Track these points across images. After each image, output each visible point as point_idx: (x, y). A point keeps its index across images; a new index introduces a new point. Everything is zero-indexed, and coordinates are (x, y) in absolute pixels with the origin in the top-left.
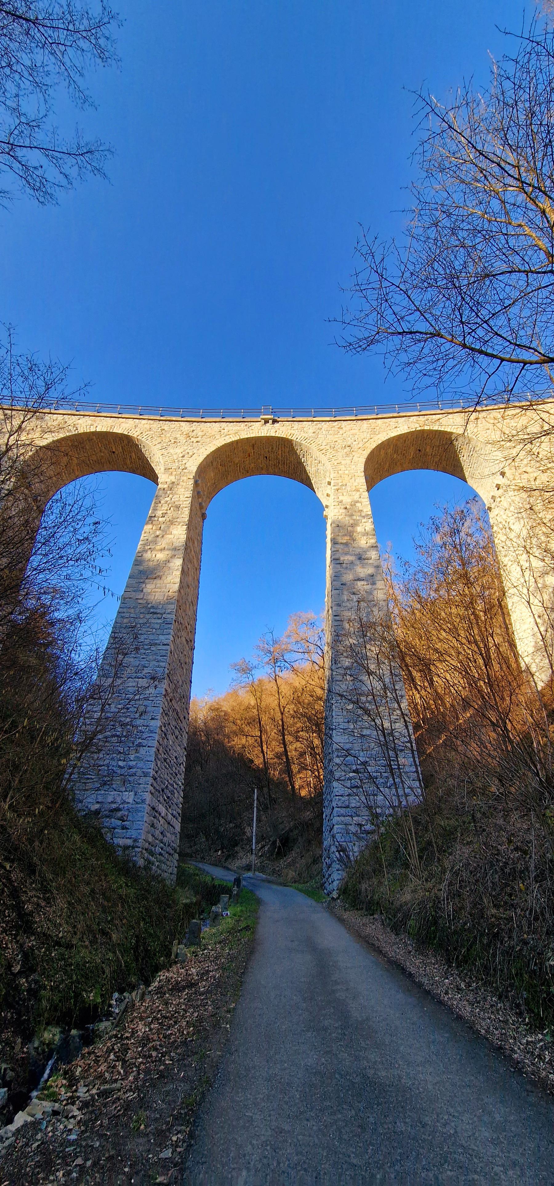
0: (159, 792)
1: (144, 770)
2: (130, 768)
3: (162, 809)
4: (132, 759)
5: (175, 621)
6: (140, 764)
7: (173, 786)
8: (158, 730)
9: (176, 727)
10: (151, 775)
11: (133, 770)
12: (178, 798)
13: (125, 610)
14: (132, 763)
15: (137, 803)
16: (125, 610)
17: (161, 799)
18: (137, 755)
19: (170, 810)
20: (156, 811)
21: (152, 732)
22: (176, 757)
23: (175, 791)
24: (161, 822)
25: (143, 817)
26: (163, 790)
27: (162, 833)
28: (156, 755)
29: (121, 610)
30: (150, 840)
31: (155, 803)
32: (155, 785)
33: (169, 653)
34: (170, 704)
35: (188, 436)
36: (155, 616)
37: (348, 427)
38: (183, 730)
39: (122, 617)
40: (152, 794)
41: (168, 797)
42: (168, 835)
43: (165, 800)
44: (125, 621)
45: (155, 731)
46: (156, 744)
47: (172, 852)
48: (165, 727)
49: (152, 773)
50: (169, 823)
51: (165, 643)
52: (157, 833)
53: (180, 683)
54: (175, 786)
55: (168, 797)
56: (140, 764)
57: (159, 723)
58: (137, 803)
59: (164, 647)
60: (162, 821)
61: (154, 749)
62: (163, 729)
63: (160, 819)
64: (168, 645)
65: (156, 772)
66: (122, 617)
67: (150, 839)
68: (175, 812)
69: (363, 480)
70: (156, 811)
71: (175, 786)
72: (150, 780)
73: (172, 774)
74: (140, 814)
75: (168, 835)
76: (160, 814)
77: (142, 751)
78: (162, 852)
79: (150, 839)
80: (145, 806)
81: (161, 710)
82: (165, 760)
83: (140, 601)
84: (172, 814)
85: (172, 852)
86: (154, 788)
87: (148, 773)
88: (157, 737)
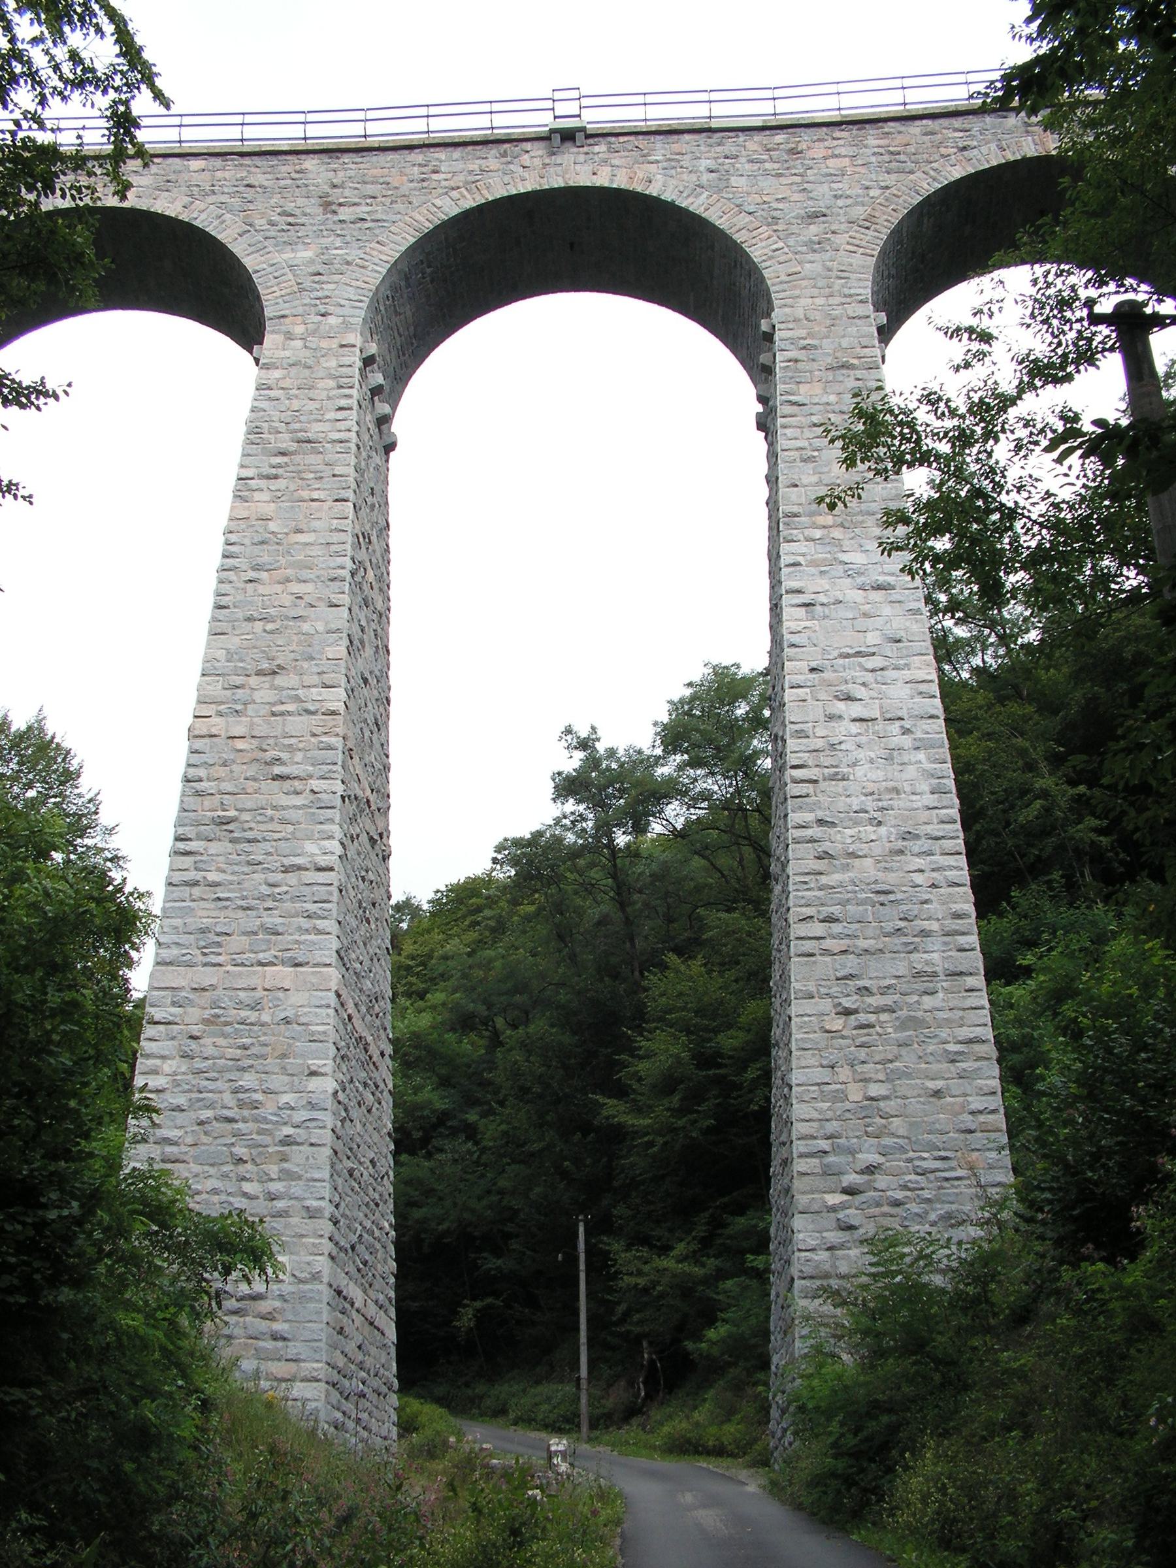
0: (342, 1252)
1: (308, 1203)
2: (272, 1197)
3: (354, 1292)
4: (274, 1176)
5: (343, 797)
6: (297, 1189)
7: (371, 1233)
8: (329, 1103)
9: (365, 1085)
10: (327, 1215)
11: (280, 1204)
12: (385, 1261)
13: (202, 772)
14: (276, 1187)
15: (301, 1281)
16: (202, 772)
17: (352, 1269)
18: (285, 1165)
19: (370, 1292)
20: (345, 1298)
21: (312, 1106)
22: (372, 1161)
23: (378, 1246)
24: (357, 1323)
25: (319, 1313)
26: (353, 1248)
27: (359, 1347)
28: (333, 1166)
29: (192, 771)
30: (340, 1365)
31: (343, 1282)
32: (337, 1237)
33: (336, 892)
34: (349, 1027)
35: (328, 206)
36: (287, 785)
37: (818, 151)
38: (382, 1086)
39: (198, 794)
40: (332, 1258)
41: (365, 1263)
42: (373, 1350)
43: (359, 1270)
44: (208, 802)
45: (322, 1105)
46: (327, 1136)
47: (384, 1389)
48: (344, 1090)
49: (329, 1209)
50: (371, 1324)
51: (323, 864)
52: (351, 1347)
53: (367, 963)
54: (377, 1233)
55: (365, 1263)
56: (297, 1189)
57: (330, 1085)
58: (301, 1281)
59: (322, 877)
60: (359, 1319)
61: (328, 1152)
62: (341, 1096)
63: (354, 1314)
64: (331, 869)
65: (337, 1206)
66: (198, 794)
67: (341, 1362)
68: (381, 1297)
69: (959, 869)
70: (345, 1298)
71: (377, 1233)
72: (327, 1227)
73: (367, 1205)
74: (311, 1305)
75: (373, 1350)
76: (352, 1304)
77: (298, 1154)
78: (366, 1390)
79: (341, 1362)
80: (320, 1287)
81: (332, 1051)
82: (351, 1173)
83: (240, 744)
84: (376, 1302)
85: (384, 1389)
86: (337, 1244)
87: (319, 1210)
88: (328, 1119)
